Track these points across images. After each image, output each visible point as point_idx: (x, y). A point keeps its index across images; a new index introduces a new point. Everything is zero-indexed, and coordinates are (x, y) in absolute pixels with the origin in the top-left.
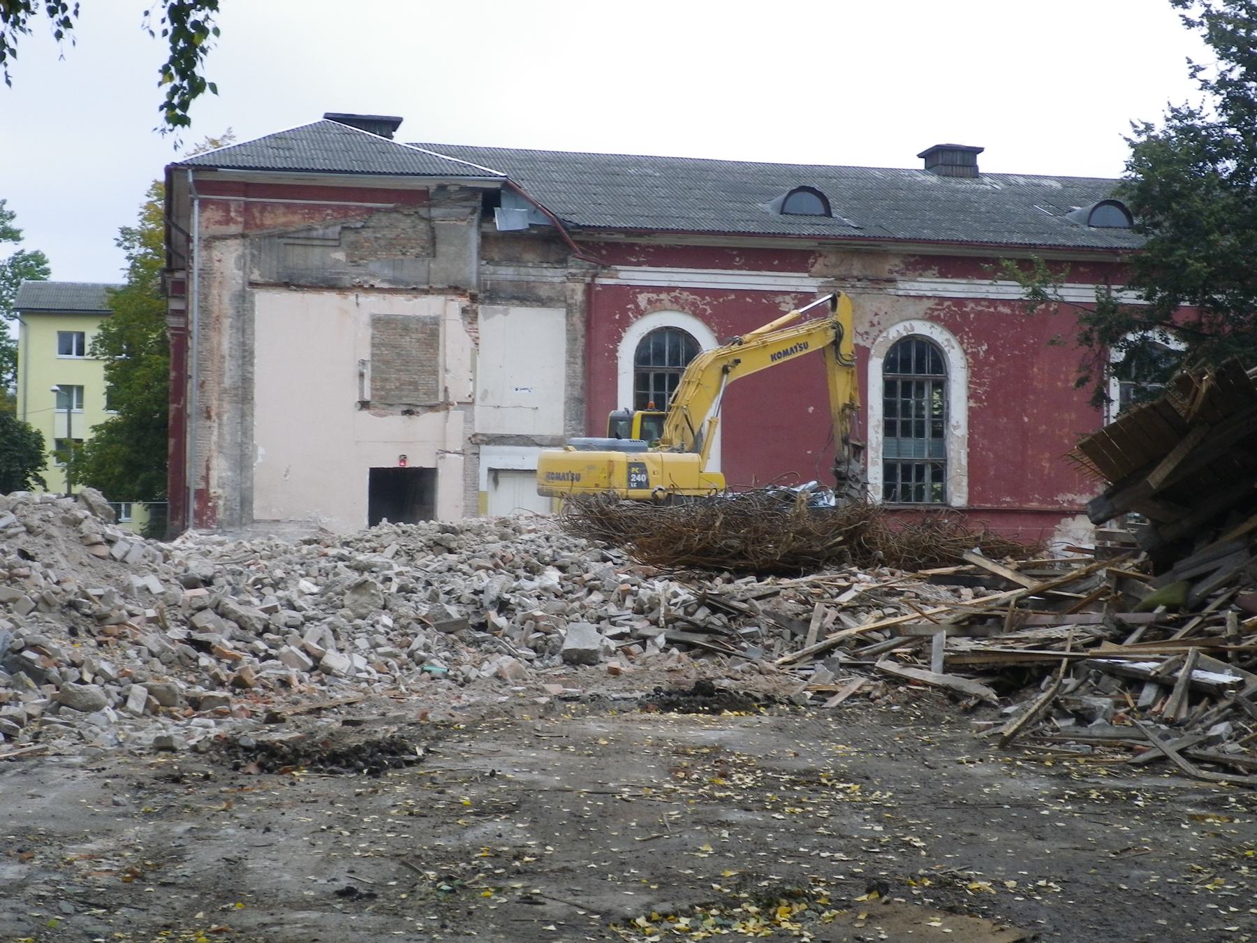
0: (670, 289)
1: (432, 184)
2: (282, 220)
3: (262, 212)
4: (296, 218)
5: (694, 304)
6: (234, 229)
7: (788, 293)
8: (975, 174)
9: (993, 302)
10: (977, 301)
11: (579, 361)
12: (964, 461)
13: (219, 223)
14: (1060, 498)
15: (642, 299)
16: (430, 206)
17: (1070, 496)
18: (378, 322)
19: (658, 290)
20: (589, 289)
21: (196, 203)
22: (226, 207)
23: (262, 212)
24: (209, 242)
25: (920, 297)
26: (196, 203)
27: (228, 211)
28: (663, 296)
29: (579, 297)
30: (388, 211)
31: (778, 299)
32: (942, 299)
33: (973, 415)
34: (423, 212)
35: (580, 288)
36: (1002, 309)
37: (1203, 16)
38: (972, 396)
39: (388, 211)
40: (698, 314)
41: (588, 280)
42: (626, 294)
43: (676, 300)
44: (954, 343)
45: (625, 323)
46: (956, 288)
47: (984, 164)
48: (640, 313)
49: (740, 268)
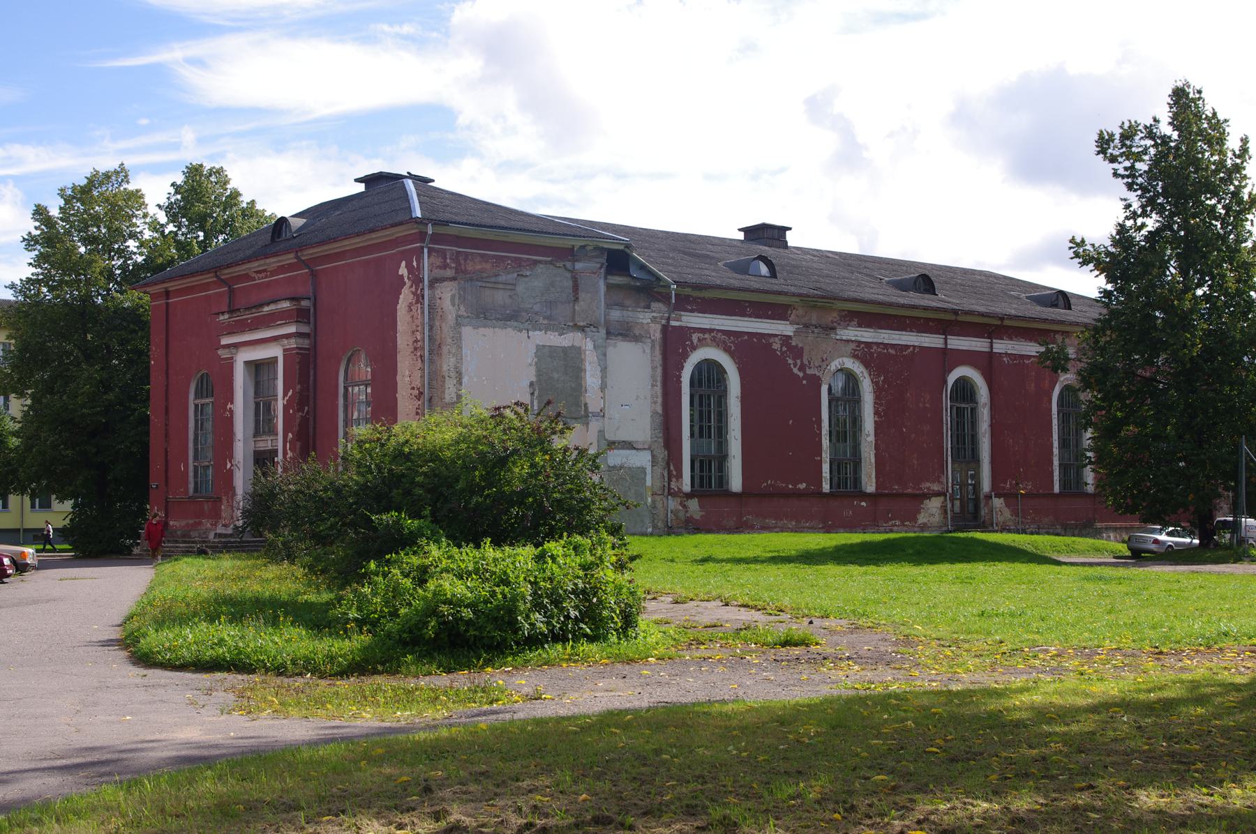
0: (710, 331)
1: (578, 243)
2: (478, 267)
3: (465, 260)
4: (488, 266)
5: (724, 342)
6: (449, 273)
7: (776, 336)
8: (784, 244)
9: (886, 346)
10: (878, 344)
11: (659, 384)
12: (873, 460)
13: (440, 267)
14: (923, 486)
15: (695, 337)
16: (574, 261)
17: (928, 484)
18: (540, 348)
19: (703, 331)
20: (665, 329)
21: (426, 250)
22: (443, 254)
23: (465, 260)
24: (433, 282)
25: (848, 341)
26: (426, 250)
27: (445, 258)
28: (707, 336)
29: (658, 335)
30: (546, 262)
31: (772, 340)
32: (860, 343)
33: (878, 427)
34: (569, 265)
35: (659, 327)
36: (892, 351)
37: (1146, 127)
38: (876, 413)
39: (546, 262)
40: (727, 350)
41: (664, 322)
42: (686, 332)
43: (714, 339)
44: (866, 374)
45: (685, 356)
46: (867, 335)
47: (792, 239)
48: (694, 348)
49: (750, 316)
